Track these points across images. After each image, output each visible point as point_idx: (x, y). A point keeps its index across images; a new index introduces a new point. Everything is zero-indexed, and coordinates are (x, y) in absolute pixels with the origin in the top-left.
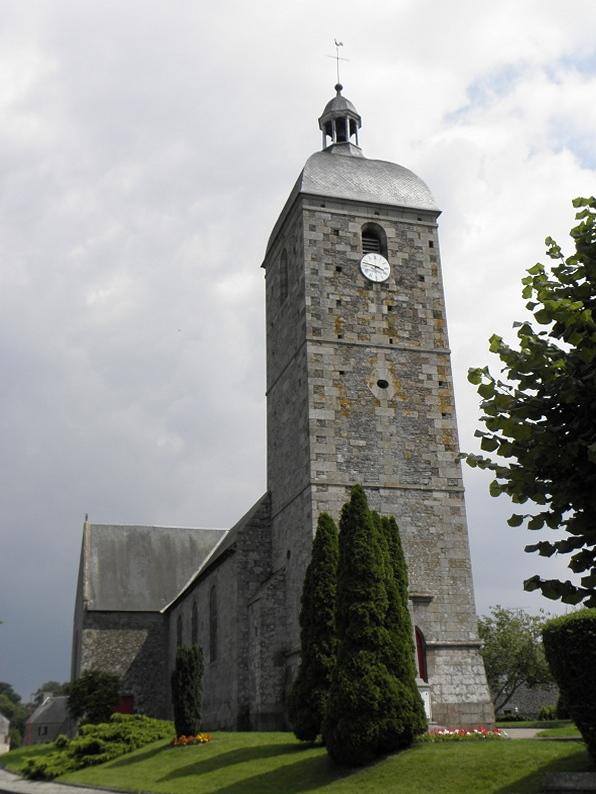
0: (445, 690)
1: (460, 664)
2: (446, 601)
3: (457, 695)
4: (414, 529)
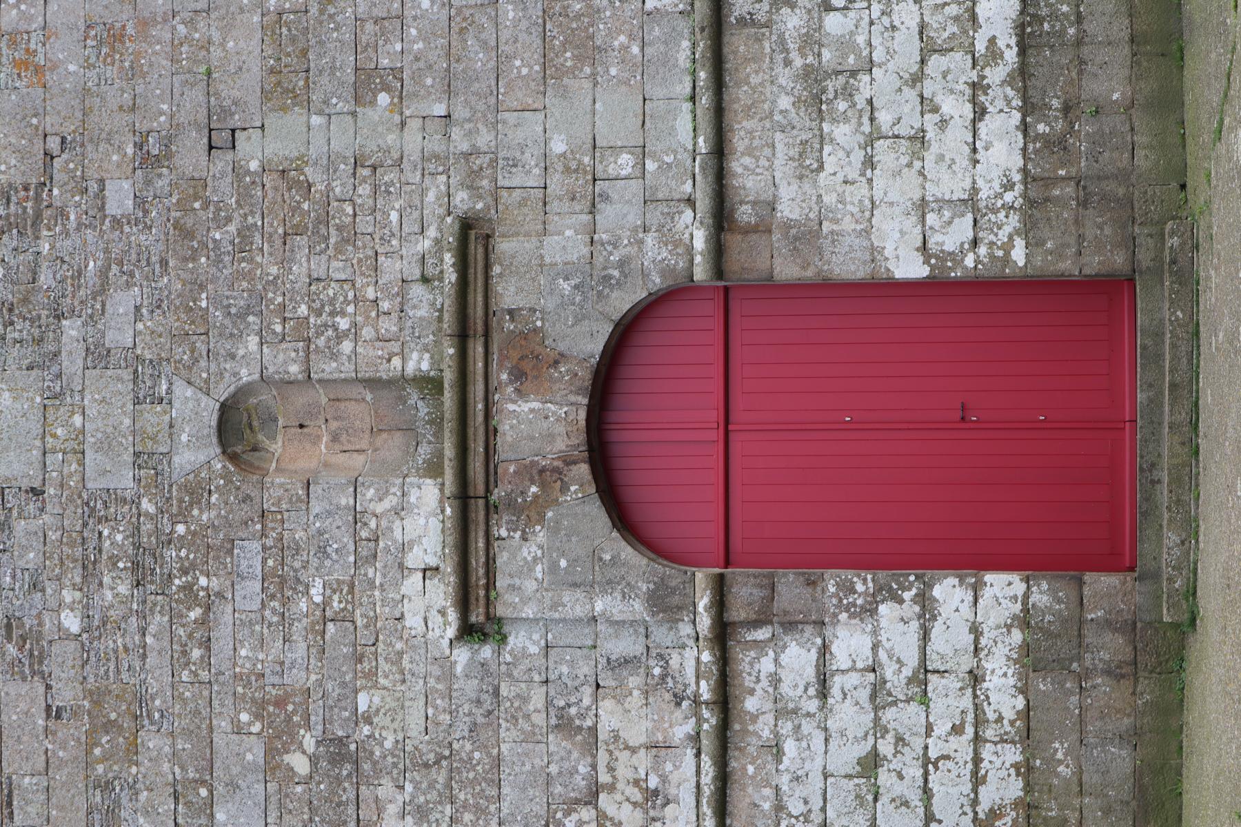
0: (952, 185)
1: (813, 77)
2: (484, 139)
3: (980, 113)
4: (122, 302)
